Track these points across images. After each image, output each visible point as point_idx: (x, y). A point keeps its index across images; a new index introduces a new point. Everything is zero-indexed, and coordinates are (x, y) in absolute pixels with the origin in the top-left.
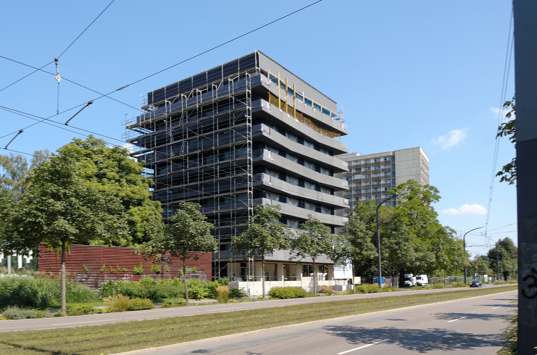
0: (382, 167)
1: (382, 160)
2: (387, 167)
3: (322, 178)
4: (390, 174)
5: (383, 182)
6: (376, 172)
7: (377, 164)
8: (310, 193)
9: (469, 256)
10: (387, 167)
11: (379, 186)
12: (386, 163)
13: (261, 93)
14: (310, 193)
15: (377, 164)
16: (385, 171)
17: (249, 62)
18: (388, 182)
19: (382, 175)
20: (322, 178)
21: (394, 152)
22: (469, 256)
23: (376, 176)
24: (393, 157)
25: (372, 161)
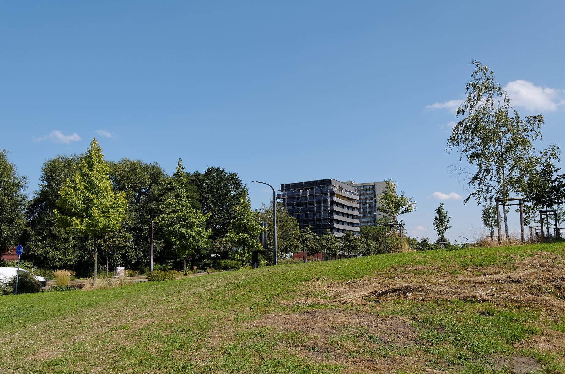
0: (368, 192)
1: (368, 187)
2: (371, 192)
3: (350, 220)
4: (372, 196)
5: (368, 201)
6: (364, 195)
7: (364, 190)
8: (345, 211)
9: (18, 185)
10: (371, 192)
11: (366, 203)
12: (370, 189)
13: (333, 194)
14: (345, 211)
15: (364, 190)
16: (369, 194)
17: (328, 182)
18: (371, 201)
19: (368, 196)
20: (350, 220)
21: (375, 183)
22: (18, 185)
23: (364, 197)
24: (374, 186)
25: (362, 188)
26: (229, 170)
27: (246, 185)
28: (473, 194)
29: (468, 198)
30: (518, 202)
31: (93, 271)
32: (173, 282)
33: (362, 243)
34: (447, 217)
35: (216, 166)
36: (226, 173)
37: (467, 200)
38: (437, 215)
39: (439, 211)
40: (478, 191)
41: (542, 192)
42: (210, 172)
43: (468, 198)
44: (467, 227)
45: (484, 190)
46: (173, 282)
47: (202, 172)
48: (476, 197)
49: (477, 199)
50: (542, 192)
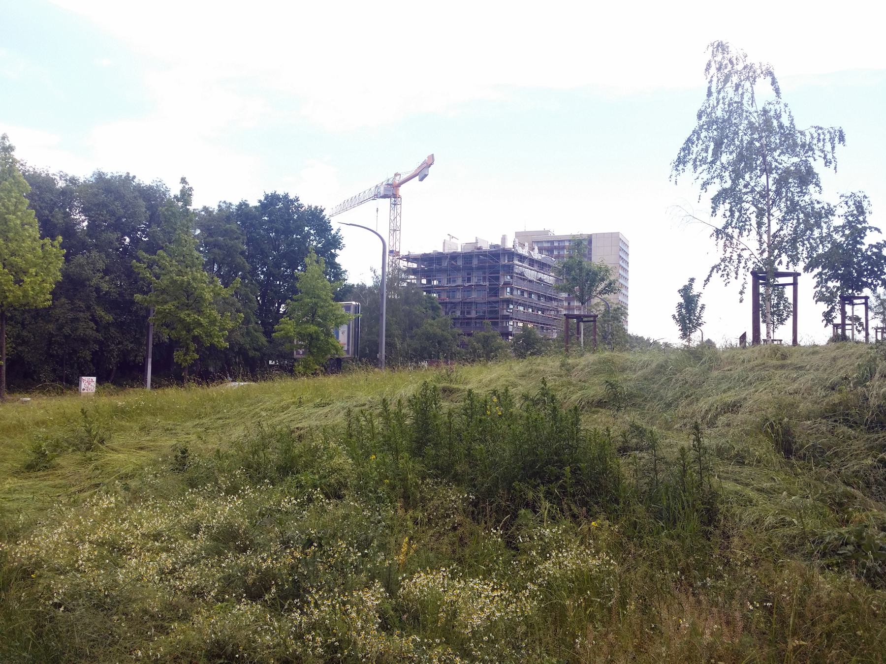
26: (308, 201)
27: (339, 230)
28: (716, 268)
29: (710, 276)
30: (863, 301)
31: (144, 380)
32: (96, 468)
33: (162, 542)
34: (700, 304)
35: (281, 192)
36: (301, 206)
37: (708, 280)
38: (682, 300)
39: (686, 292)
40: (723, 260)
41: (847, 269)
42: (271, 201)
43: (710, 276)
44: (727, 320)
45: (735, 257)
46: (96, 468)
47: (253, 203)
48: (720, 272)
49: (722, 275)
50: (847, 269)
